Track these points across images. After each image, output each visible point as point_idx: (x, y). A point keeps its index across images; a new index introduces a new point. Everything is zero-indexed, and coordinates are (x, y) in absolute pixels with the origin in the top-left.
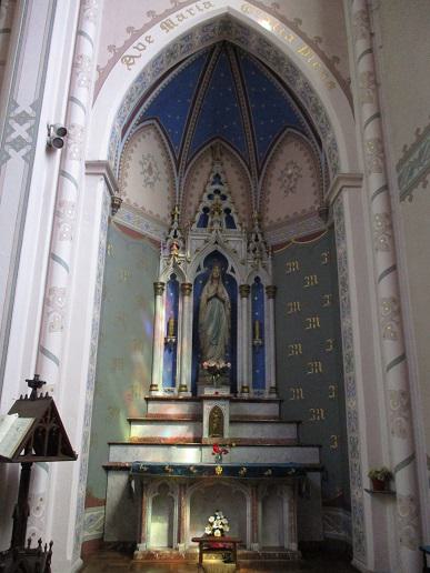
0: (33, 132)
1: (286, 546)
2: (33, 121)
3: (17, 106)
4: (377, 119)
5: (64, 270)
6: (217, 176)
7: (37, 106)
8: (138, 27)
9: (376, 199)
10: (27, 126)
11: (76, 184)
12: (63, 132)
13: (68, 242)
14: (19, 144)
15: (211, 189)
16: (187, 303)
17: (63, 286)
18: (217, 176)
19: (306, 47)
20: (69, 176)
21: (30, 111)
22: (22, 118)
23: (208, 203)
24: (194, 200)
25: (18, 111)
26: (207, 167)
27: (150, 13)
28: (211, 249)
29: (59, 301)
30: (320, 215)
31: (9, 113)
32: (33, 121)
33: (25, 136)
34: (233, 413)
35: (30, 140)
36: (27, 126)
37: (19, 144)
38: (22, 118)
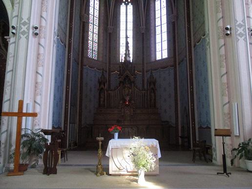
0: (28, 29)
1: (130, 129)
2: (28, 25)
3: (23, 19)
5: (45, 21)
7: (29, 19)
9: (15, 18)
10: (26, 26)
11: (45, 19)
12: (87, 83)
13: (45, 12)
14: (24, 33)
17: (45, 25)
20: (43, 18)
21: (27, 21)
25: (23, 21)
29: (40, 86)
31: (236, 33)
32: (28, 25)
33: (26, 30)
35: (27, 31)
36: (26, 26)
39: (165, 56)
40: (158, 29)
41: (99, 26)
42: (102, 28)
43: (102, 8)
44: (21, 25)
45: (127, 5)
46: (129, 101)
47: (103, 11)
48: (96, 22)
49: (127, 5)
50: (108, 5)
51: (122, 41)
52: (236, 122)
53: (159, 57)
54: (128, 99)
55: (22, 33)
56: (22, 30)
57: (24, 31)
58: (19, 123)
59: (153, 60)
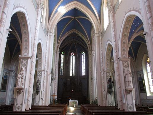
20: (30, 87)
39: (85, 75)
40: (83, 65)
41: (64, 64)
42: (64, 65)
43: (65, 58)
44: (16, 108)
45: (73, 56)
46: (73, 90)
47: (65, 59)
48: (63, 63)
49: (73, 56)
50: (84, 44)
51: (71, 69)
52: (49, 91)
53: (83, 75)
54: (73, 89)
55: (39, 75)
56: (39, 74)
57: (39, 76)
58: (54, 97)
59: (81, 75)
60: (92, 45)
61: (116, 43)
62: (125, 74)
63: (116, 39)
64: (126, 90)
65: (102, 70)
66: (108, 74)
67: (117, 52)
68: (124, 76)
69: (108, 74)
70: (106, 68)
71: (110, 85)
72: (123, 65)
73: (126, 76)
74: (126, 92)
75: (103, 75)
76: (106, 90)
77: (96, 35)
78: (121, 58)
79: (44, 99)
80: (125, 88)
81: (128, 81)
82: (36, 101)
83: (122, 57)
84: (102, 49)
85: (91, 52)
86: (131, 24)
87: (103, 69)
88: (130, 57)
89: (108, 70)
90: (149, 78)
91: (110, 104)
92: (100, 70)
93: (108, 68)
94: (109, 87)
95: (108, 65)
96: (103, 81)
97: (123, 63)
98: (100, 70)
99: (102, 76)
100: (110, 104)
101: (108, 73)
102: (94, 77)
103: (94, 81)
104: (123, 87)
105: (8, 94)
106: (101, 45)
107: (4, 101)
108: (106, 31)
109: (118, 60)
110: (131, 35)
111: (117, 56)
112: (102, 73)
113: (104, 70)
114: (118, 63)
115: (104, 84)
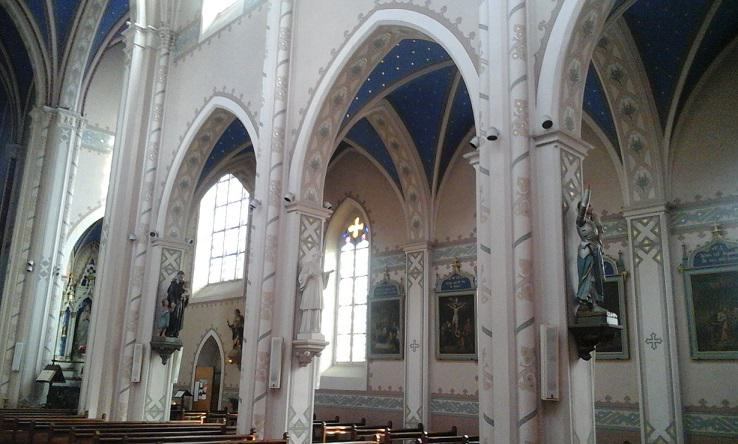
0: (49, 269)
4: (524, 82)
6: (93, 260)
7: (51, 259)
8: (83, 214)
14: (44, 274)
15: (89, 266)
16: (73, 321)
18: (93, 260)
19: (107, 420)
22: (45, 263)
23: (88, 274)
24: (80, 271)
26: (88, 254)
27: (80, 215)
28: (86, 296)
30: (429, 245)
34: (573, 325)
37: (44, 274)
38: (45, 263)
60: (70, 77)
61: (284, 122)
62: (303, 277)
63: (165, 87)
64: (293, 345)
65: (139, 231)
66: (171, 259)
67: (281, 164)
68: (298, 284)
69: (171, 259)
70: (167, 227)
71: (172, 314)
72: (301, 233)
73: (304, 288)
74: (292, 355)
75: (140, 259)
76: (146, 338)
77: (139, 39)
78: (298, 198)
79: (125, 383)
80: (294, 337)
81: (314, 310)
82: (294, 406)
83: (302, 195)
84: (160, 121)
85: (55, 117)
86: (378, 58)
87: (148, 225)
88: (328, 205)
89: (174, 235)
90: (340, 303)
91: (150, 411)
92: (131, 230)
93: (174, 229)
94: (165, 322)
95: (177, 210)
96: (135, 292)
97: (302, 223)
98: (131, 230)
99: (138, 262)
100: (150, 411)
101: (172, 252)
102: (46, 258)
103: (43, 279)
104: (286, 332)
105: (410, 368)
106: (158, 99)
107: (629, 420)
108: (209, 39)
109: (278, 206)
110: (354, 108)
111: (279, 183)
112: (140, 248)
113: (153, 234)
114: (277, 218)
115: (139, 307)
